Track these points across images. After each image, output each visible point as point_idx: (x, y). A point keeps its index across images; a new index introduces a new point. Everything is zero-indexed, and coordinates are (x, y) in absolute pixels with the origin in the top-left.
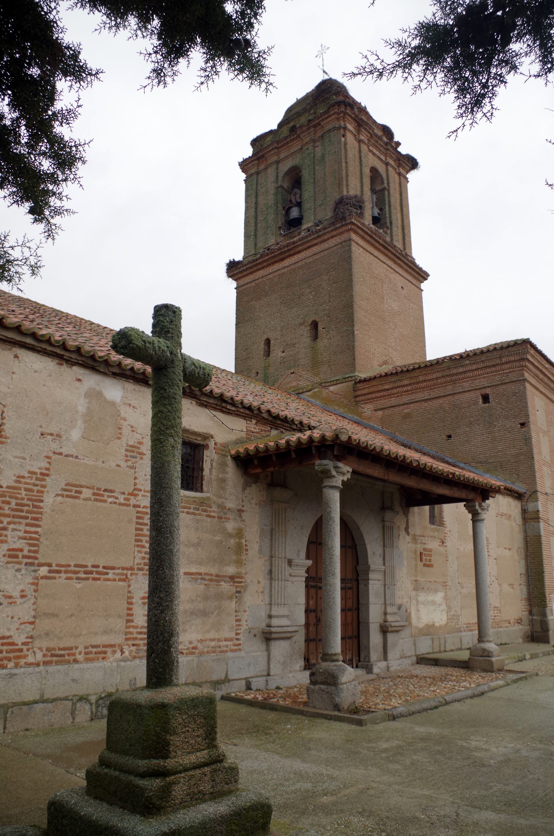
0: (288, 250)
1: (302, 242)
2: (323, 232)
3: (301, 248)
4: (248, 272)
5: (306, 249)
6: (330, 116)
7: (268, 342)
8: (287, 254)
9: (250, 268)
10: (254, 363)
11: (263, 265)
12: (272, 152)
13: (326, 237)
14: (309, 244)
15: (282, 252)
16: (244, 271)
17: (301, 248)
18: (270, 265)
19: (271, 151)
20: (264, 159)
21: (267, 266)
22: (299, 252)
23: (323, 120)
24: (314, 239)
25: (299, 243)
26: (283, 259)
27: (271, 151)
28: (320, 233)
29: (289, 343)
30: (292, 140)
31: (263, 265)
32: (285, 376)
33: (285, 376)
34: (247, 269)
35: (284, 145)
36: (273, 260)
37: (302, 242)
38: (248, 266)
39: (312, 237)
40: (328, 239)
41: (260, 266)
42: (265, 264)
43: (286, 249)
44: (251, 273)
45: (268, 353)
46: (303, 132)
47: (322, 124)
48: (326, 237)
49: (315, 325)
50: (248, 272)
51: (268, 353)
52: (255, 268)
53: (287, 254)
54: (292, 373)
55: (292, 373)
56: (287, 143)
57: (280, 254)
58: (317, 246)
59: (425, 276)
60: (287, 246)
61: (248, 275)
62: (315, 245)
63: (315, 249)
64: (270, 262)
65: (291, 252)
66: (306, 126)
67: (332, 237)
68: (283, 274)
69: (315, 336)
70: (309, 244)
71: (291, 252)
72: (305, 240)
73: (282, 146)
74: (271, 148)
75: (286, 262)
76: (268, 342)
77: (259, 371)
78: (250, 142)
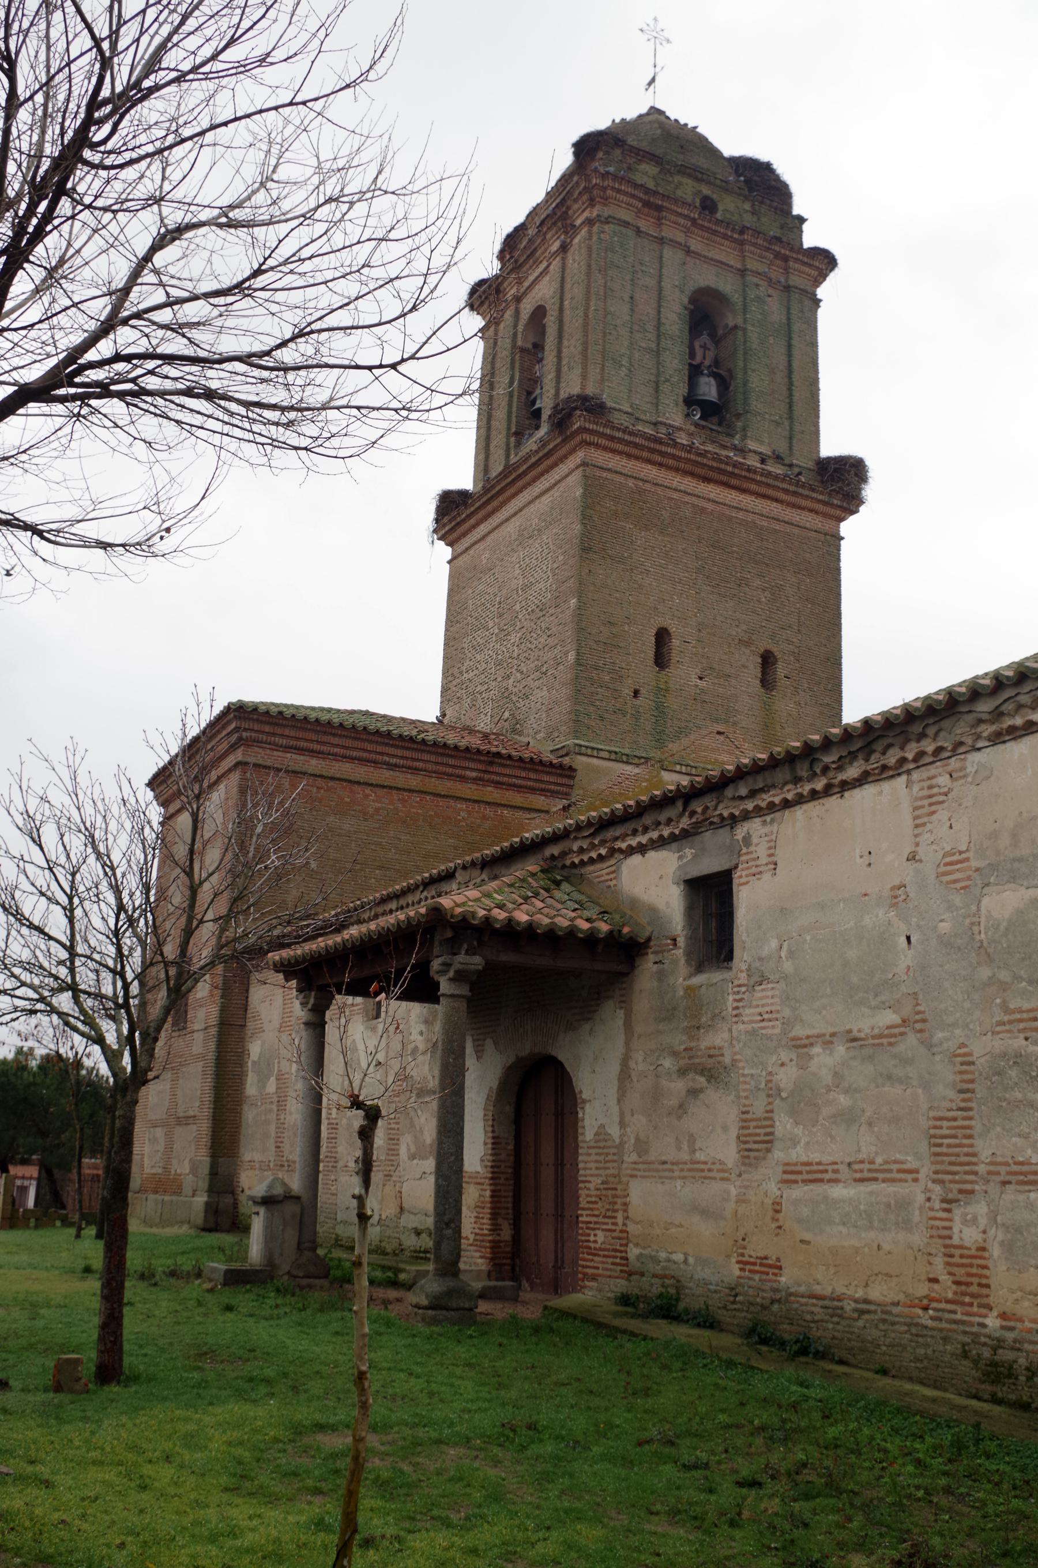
0: (732, 474)
1: (763, 479)
2: (806, 492)
3: (753, 487)
4: (627, 449)
5: (758, 495)
6: (810, 266)
7: (662, 637)
8: (725, 478)
9: (636, 445)
10: (628, 664)
11: (665, 461)
12: (682, 221)
13: (804, 503)
14: (770, 492)
15: (718, 468)
16: (620, 441)
17: (753, 487)
18: (677, 470)
19: (680, 215)
20: (656, 214)
21: (669, 468)
22: (743, 491)
23: (796, 260)
24: (786, 491)
25: (758, 478)
26: (706, 480)
27: (680, 215)
28: (800, 490)
29: (715, 666)
30: (725, 237)
31: (665, 461)
32: (704, 732)
33: (704, 732)
34: (628, 443)
35: (708, 230)
36: (688, 467)
37: (763, 479)
38: (637, 440)
39: (785, 486)
40: (803, 508)
41: (658, 458)
42: (671, 462)
43: (730, 469)
44: (629, 456)
45: (661, 660)
46: (755, 245)
47: (791, 264)
48: (804, 503)
49: (767, 660)
50: (627, 449)
51: (661, 660)
52: (645, 454)
53: (725, 478)
54: (719, 733)
55: (719, 733)
56: (715, 233)
57: (711, 468)
58: (779, 506)
59: (451, 538)
60: (734, 466)
61: (620, 453)
62: (777, 500)
63: (775, 508)
64: (682, 465)
65: (734, 482)
66: (765, 240)
67: (811, 510)
68: (703, 510)
69: (767, 681)
70: (770, 492)
71: (734, 482)
72: (770, 481)
73: (702, 228)
74: (686, 212)
75: (713, 491)
76: (662, 637)
77: (643, 691)
78: (575, 137)
